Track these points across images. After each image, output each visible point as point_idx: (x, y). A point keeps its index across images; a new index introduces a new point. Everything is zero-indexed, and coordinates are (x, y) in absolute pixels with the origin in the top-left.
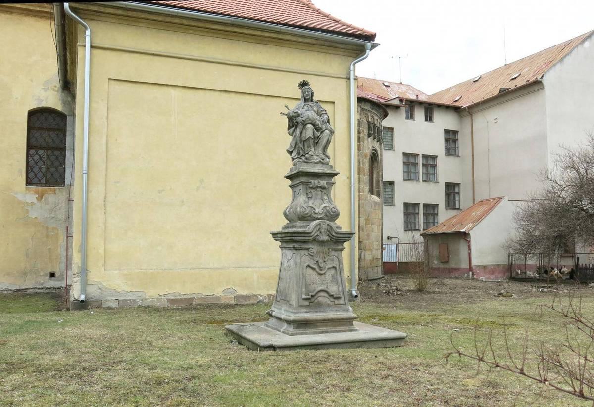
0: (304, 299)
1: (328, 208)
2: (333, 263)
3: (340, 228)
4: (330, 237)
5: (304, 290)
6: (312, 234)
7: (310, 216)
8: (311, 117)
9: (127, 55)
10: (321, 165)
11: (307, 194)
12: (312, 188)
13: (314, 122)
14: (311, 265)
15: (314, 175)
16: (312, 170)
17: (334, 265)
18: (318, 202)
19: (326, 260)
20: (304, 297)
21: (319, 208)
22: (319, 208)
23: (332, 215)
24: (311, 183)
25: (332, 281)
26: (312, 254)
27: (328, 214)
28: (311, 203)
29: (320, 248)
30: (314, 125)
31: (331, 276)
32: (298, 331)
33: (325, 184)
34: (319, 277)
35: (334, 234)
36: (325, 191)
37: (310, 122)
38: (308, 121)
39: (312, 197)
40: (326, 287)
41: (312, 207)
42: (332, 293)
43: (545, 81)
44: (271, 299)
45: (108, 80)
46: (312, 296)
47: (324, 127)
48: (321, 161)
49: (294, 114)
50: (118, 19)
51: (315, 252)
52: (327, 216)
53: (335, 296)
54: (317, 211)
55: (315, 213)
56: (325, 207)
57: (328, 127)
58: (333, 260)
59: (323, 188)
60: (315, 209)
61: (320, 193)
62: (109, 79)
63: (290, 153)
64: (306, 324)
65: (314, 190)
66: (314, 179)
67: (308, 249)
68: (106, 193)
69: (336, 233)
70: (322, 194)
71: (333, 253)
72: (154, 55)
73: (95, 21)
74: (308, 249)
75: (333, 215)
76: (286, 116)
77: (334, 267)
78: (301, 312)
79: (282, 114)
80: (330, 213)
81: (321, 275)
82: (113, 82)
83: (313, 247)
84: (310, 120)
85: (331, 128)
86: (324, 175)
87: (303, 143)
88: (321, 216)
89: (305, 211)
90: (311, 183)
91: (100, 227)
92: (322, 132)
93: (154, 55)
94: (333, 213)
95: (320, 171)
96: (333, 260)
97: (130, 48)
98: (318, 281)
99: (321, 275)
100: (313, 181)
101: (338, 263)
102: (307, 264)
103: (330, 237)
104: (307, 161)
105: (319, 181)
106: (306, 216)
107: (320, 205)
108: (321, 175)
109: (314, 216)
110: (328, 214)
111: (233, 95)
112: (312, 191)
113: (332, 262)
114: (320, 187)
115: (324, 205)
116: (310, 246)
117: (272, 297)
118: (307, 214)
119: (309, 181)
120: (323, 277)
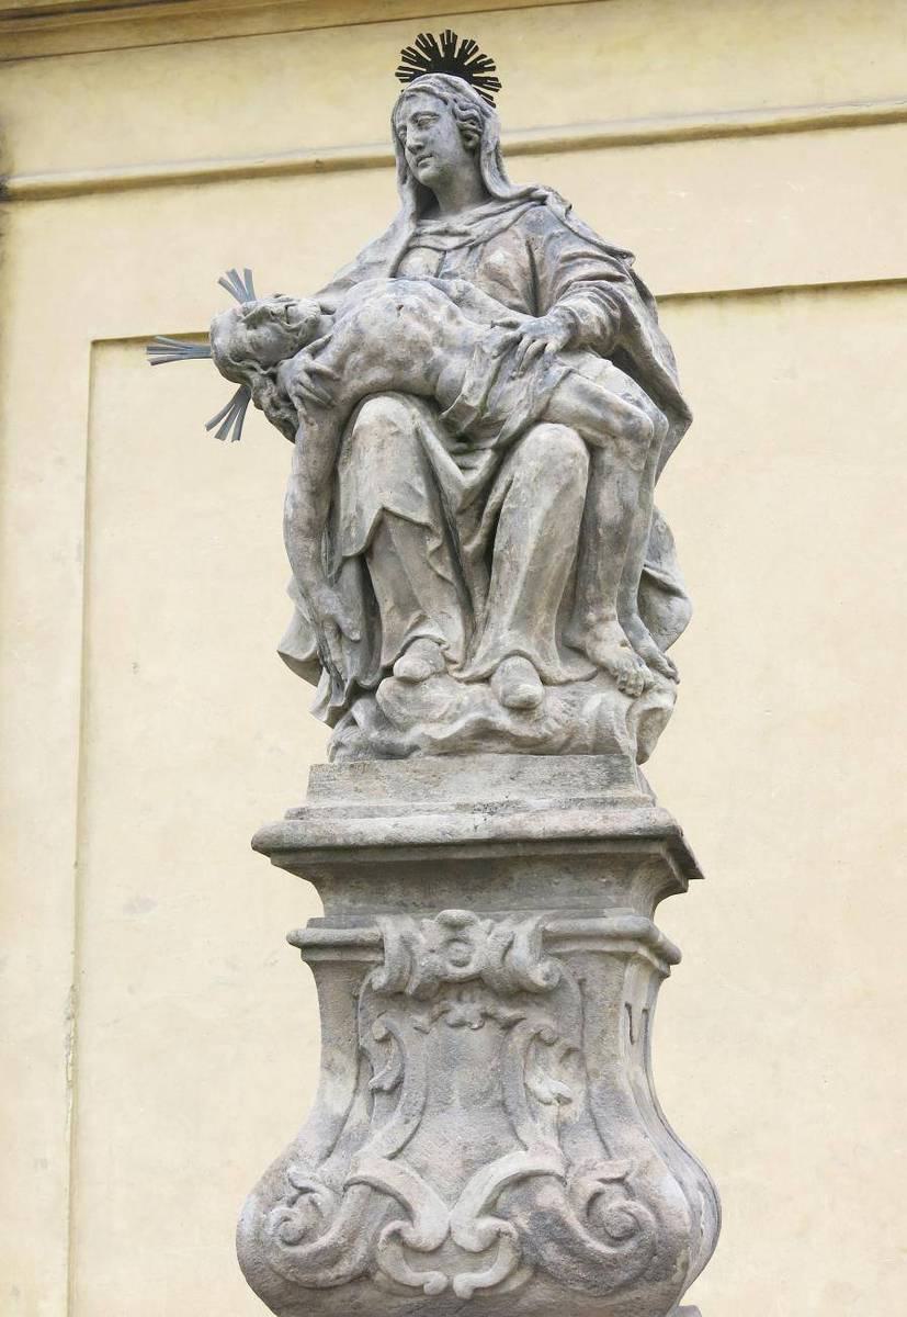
7: (363, 1276)
8: (375, 334)
9: (187, 198)
10: (506, 762)
11: (362, 1056)
12: (394, 996)
13: (417, 369)
15: (425, 866)
16: (379, 829)
18: (451, 1131)
21: (453, 1198)
22: (453, 1198)
23: (594, 1263)
24: (378, 946)
27: (550, 1253)
28: (372, 1163)
30: (432, 400)
33: (522, 953)
36: (539, 1019)
37: (377, 374)
38: (362, 369)
39: (398, 1084)
41: (378, 1189)
45: (89, 347)
47: (515, 401)
48: (504, 721)
49: (245, 335)
50: (135, 22)
52: (539, 1269)
54: (426, 1230)
55: (414, 1252)
56: (522, 1180)
57: (566, 399)
60: (406, 1211)
61: (479, 1040)
62: (95, 343)
63: (310, 668)
65: (422, 1019)
66: (402, 908)
68: (78, 972)
70: (500, 1050)
72: (320, 168)
73: (29, 66)
75: (614, 1263)
80: (568, 1243)
82: (116, 354)
84: (374, 358)
85: (597, 400)
86: (530, 861)
87: (351, 572)
88: (486, 1277)
89: (304, 1237)
90: (378, 946)
91: (44, 1163)
92: (505, 451)
93: (320, 168)
94: (616, 1241)
95: (471, 826)
97: (209, 159)
100: (390, 928)
104: (389, 737)
105: (455, 926)
107: (470, 1167)
109: (411, 1276)
110: (550, 1253)
111: (801, 308)
112: (405, 1026)
114: (477, 982)
118: (333, 1256)
119: (365, 934)
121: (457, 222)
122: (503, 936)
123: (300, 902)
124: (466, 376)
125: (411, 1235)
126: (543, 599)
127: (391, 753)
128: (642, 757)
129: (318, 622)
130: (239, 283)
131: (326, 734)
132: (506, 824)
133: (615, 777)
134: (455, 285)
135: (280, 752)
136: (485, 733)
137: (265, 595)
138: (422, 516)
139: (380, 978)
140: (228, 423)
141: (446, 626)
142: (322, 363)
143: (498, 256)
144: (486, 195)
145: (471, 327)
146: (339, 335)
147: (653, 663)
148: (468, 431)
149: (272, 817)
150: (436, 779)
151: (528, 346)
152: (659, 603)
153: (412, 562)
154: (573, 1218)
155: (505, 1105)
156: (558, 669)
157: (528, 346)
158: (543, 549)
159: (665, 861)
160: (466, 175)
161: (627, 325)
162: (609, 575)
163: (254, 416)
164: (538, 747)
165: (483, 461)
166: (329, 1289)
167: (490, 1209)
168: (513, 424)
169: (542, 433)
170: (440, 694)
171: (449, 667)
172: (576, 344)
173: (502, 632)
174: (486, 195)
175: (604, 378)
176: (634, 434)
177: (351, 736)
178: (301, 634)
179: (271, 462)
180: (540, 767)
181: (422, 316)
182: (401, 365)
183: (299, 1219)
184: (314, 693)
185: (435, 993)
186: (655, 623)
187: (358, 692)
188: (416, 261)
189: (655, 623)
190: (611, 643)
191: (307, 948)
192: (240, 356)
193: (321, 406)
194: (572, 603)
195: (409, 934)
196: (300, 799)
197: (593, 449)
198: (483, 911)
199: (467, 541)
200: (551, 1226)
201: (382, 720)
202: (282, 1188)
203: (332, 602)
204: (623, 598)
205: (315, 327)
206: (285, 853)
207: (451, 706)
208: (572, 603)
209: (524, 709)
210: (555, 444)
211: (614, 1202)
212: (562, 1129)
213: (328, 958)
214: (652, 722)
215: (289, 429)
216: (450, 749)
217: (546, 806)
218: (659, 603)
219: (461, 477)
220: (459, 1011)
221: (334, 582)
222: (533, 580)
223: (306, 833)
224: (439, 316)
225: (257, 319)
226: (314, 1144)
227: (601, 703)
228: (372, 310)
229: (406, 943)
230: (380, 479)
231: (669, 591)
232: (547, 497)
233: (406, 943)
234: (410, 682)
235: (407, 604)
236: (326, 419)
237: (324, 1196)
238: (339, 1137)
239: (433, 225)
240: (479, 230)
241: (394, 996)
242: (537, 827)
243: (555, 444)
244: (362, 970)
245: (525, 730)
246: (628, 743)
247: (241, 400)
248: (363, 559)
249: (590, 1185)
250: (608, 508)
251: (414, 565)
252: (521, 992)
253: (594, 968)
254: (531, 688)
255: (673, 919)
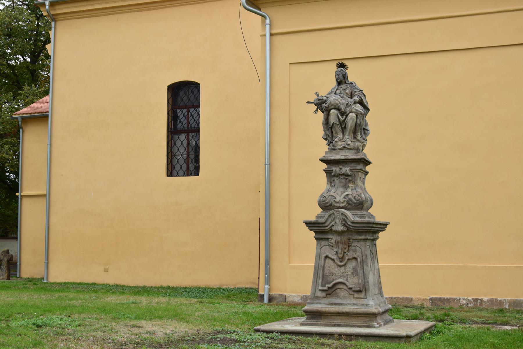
0: (320, 290)
1: (350, 196)
2: (356, 254)
3: (374, 218)
4: (347, 227)
5: (320, 281)
6: (326, 224)
8: (332, 103)
11: (331, 182)
12: (334, 176)
14: (330, 256)
16: (333, 158)
17: (355, 256)
19: (345, 251)
20: (320, 288)
24: (332, 171)
25: (353, 273)
26: (331, 244)
27: (350, 202)
28: (332, 193)
29: (338, 239)
30: (339, 109)
31: (352, 268)
32: (309, 322)
33: (348, 171)
34: (339, 268)
35: (349, 223)
36: (350, 178)
37: (333, 107)
40: (345, 279)
41: (332, 196)
42: (351, 286)
43: (335, 84)
44: (479, 304)
46: (329, 288)
47: (348, 110)
48: (347, 146)
51: (334, 243)
52: (349, 204)
53: (353, 289)
54: (338, 199)
55: (336, 202)
56: (347, 195)
57: (353, 110)
58: (355, 251)
59: (346, 175)
60: (335, 198)
61: (343, 181)
63: (326, 139)
64: (321, 315)
66: (335, 167)
67: (327, 239)
69: (353, 223)
71: (356, 244)
74: (327, 239)
76: (313, 104)
77: (355, 258)
78: (314, 303)
79: (308, 103)
81: (341, 266)
83: (331, 237)
84: (332, 105)
85: (357, 110)
88: (344, 205)
89: (325, 201)
90: (332, 171)
92: (347, 116)
95: (343, 158)
96: (355, 251)
98: (337, 273)
99: (341, 266)
100: (334, 169)
101: (360, 254)
102: (325, 255)
103: (347, 227)
106: (327, 205)
107: (342, 193)
108: (347, 162)
112: (335, 179)
113: (354, 253)
114: (343, 174)
115: (346, 193)
116: (330, 236)
117: (479, 301)
118: (327, 203)
119: (331, 169)
120: (343, 268)
121: (342, 86)
122: (346, 169)
123: (325, 166)
124: (343, 108)
125: (336, 200)
126: (351, 132)
127: (334, 150)
128: (363, 150)
129: (326, 134)
130: (317, 94)
131: (328, 147)
132: (346, 157)
133: (358, 152)
134: (342, 95)
135: (322, 148)
136: (344, 147)
137: (320, 131)
138: (338, 123)
139: (333, 174)
140: (316, 112)
141: (340, 136)
142: (326, 106)
143: (347, 91)
144: (346, 83)
145: (344, 101)
146: (328, 102)
147: (364, 139)
148: (343, 113)
149: (321, 157)
150: (339, 153)
151: (349, 104)
152: (366, 131)
153: (337, 128)
154: (353, 199)
155: (346, 187)
156: (353, 140)
157: (349, 104)
158: (351, 127)
159: (367, 163)
160: (344, 81)
161: (362, 100)
162: (360, 130)
163: (319, 111)
164: (350, 149)
165: (344, 117)
166: (327, 206)
167: (344, 198)
168: (348, 113)
169: (351, 114)
170: (340, 143)
171: (340, 139)
172: (355, 103)
173: (347, 136)
174: (346, 83)
175: (359, 107)
176: (361, 114)
177: (330, 148)
178: (324, 135)
179: (321, 115)
180: (351, 151)
181: (337, 100)
182: (335, 106)
183: (324, 199)
184: (326, 142)
185: (338, 176)
186: (365, 133)
187: (331, 143)
188: (338, 92)
189: (365, 133)
190: (359, 137)
191: (325, 171)
192: (317, 104)
193: (326, 110)
194: (355, 132)
195: (336, 169)
196: (324, 155)
197: (357, 115)
198: (344, 166)
199: (343, 125)
200: (350, 200)
201: (333, 146)
202: (322, 196)
203: (328, 133)
204: (361, 132)
205: (326, 101)
206: (323, 161)
207: (340, 145)
208: (354, 132)
209: (349, 145)
210: (352, 115)
211: (357, 197)
212: (352, 190)
213: (328, 172)
214: (364, 146)
215: (323, 112)
216: (341, 149)
217: (351, 155)
218: (366, 131)
219: (342, 119)
220: (341, 177)
221: (328, 130)
222: (350, 130)
223: (325, 158)
224: (339, 100)
225: (319, 100)
226: (326, 192)
227: (357, 144)
228: (332, 99)
229: (336, 170)
230: (333, 119)
231: (367, 130)
232: (351, 121)
233: (336, 170)
234: (336, 142)
235: (336, 133)
236: (327, 111)
237: (327, 197)
238: (329, 191)
239: (340, 87)
240: (345, 88)
241: (334, 176)
242: (349, 158)
243: (352, 115)
244: (331, 173)
245: (349, 147)
246: (361, 148)
247: (317, 109)
248: (331, 128)
249: (354, 195)
250: (358, 122)
251: (338, 129)
252: (348, 175)
253: (356, 173)
254: (350, 143)
255: (368, 168)
